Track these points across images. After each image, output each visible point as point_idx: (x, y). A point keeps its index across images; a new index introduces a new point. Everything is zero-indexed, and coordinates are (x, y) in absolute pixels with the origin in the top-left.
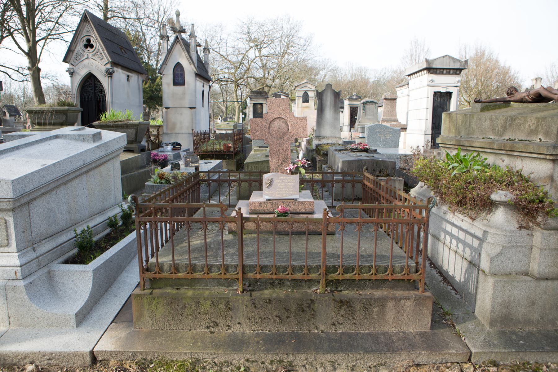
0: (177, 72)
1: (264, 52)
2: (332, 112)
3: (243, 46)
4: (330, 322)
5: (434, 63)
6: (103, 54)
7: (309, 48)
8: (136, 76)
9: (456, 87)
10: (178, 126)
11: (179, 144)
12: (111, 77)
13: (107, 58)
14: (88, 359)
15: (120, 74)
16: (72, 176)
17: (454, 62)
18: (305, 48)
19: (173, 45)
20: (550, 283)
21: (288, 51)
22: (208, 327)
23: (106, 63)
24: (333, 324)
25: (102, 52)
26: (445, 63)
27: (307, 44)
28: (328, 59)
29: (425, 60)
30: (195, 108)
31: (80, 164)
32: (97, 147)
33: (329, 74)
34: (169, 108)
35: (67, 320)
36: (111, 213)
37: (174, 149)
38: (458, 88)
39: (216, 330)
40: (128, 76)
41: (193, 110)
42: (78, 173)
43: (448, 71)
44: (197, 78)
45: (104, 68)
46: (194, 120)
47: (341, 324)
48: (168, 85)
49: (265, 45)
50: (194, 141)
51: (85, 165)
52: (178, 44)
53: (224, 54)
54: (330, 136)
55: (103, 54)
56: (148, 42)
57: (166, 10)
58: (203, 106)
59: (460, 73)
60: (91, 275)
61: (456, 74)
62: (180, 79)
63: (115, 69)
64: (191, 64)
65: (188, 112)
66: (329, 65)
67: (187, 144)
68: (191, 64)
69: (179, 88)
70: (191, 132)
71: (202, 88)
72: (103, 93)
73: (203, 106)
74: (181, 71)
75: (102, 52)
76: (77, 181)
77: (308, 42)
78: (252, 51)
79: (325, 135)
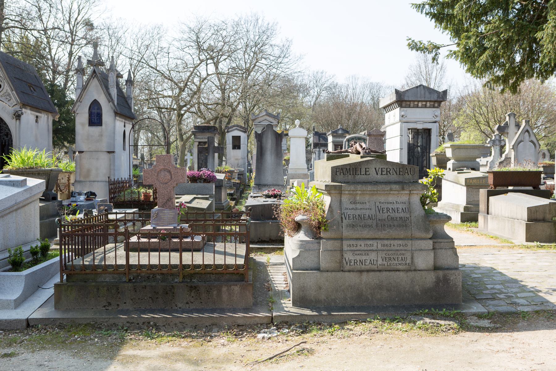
0: (93, 111)
1: (224, 66)
2: (273, 157)
3: (191, 56)
4: (185, 301)
5: (406, 95)
6: (12, 95)
7: (286, 60)
8: (46, 116)
9: (435, 122)
10: (93, 172)
11: (94, 194)
12: (20, 119)
13: (14, 98)
14: (25, 324)
15: (28, 115)
16: (7, 211)
17: (430, 93)
18: (279, 60)
19: (89, 81)
20: (329, 274)
21: (257, 64)
22: (104, 306)
23: (14, 104)
24: (187, 303)
25: (10, 93)
26: (419, 95)
27: (283, 55)
28: (322, 73)
29: (394, 91)
30: (113, 152)
31: (13, 202)
32: (24, 190)
33: (324, 94)
34: (83, 152)
35: (9, 304)
36: (34, 246)
37: (88, 199)
38: (437, 124)
39: (110, 308)
40: (37, 117)
41: (112, 154)
42: (11, 210)
43: (424, 103)
44: (117, 118)
45: (11, 110)
46: (112, 164)
47: (192, 303)
48: (83, 125)
49: (224, 57)
50: (110, 190)
51: (16, 204)
52: (95, 79)
53: (163, 69)
54: (271, 184)
55: (12, 95)
56: (53, 52)
57: (81, 8)
58: (124, 149)
59: (439, 105)
60: (23, 278)
61: (434, 107)
62: (95, 119)
63: (24, 110)
64: (109, 102)
65: (104, 158)
66: (323, 80)
67: (102, 195)
68: (109, 102)
69: (95, 130)
70: (108, 180)
71: (123, 129)
72: (9, 136)
73: (124, 149)
74: (98, 109)
75: (10, 93)
76: (9, 216)
77: (284, 53)
78: (203, 66)
79: (266, 183)
